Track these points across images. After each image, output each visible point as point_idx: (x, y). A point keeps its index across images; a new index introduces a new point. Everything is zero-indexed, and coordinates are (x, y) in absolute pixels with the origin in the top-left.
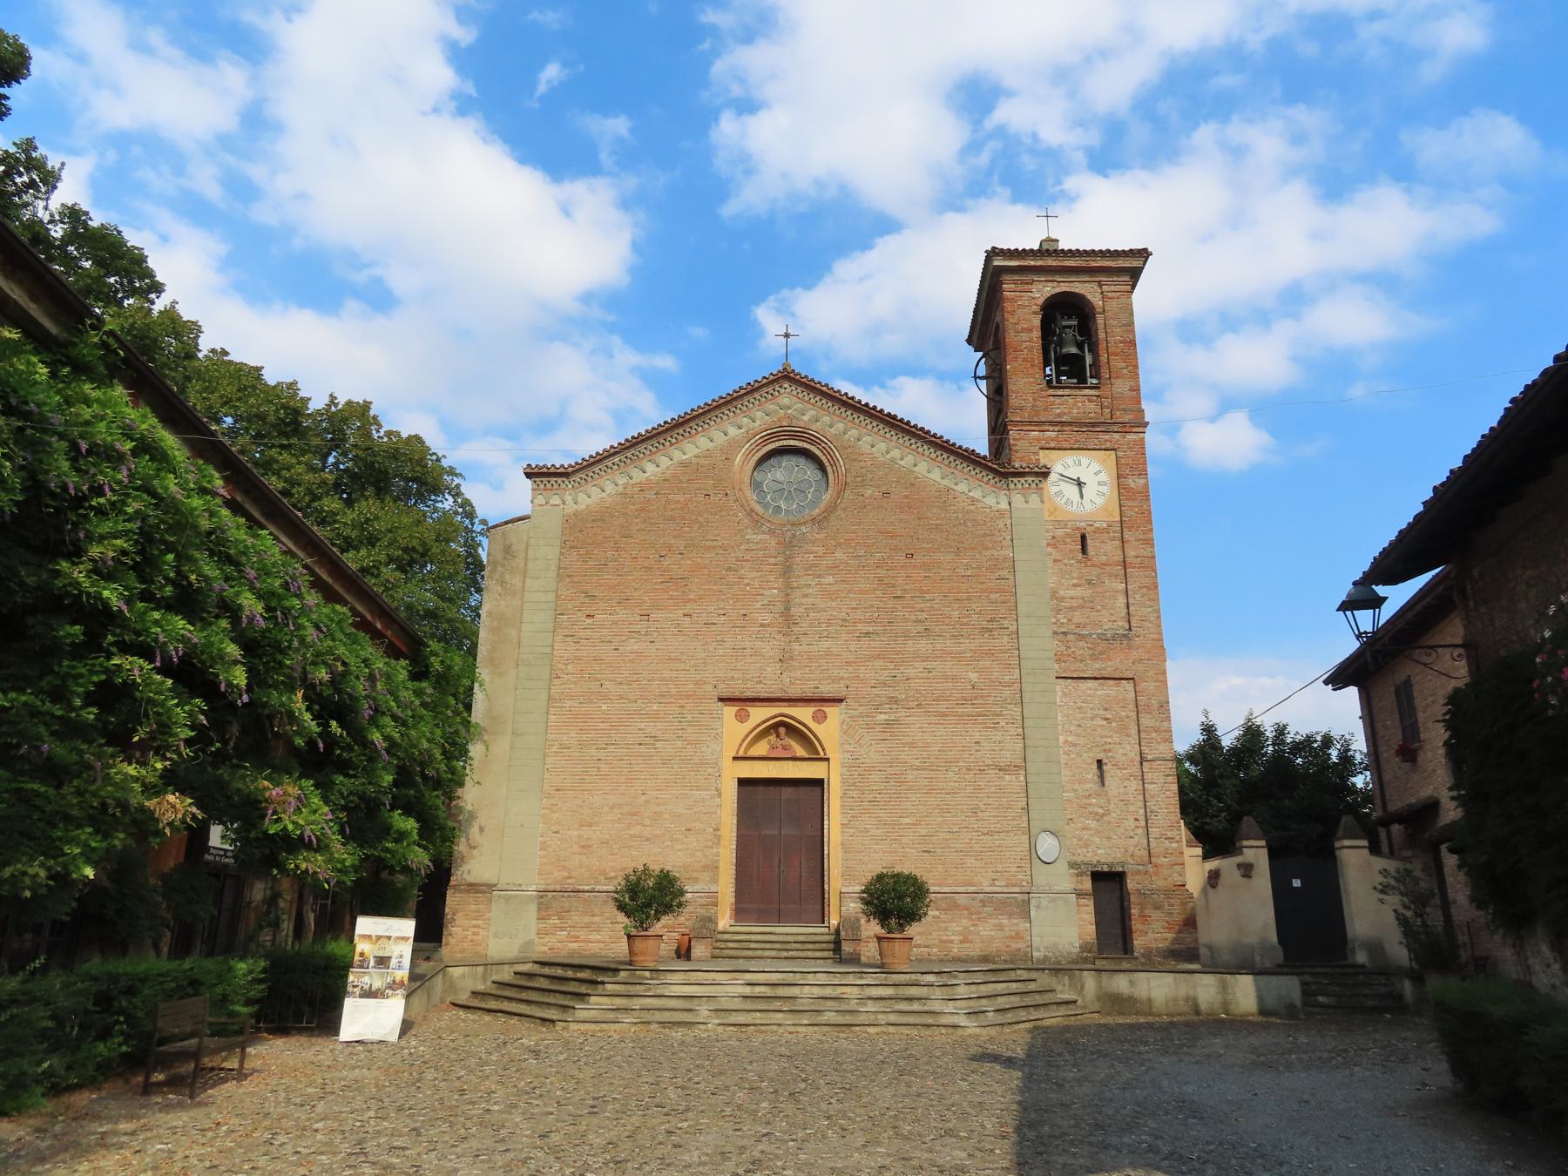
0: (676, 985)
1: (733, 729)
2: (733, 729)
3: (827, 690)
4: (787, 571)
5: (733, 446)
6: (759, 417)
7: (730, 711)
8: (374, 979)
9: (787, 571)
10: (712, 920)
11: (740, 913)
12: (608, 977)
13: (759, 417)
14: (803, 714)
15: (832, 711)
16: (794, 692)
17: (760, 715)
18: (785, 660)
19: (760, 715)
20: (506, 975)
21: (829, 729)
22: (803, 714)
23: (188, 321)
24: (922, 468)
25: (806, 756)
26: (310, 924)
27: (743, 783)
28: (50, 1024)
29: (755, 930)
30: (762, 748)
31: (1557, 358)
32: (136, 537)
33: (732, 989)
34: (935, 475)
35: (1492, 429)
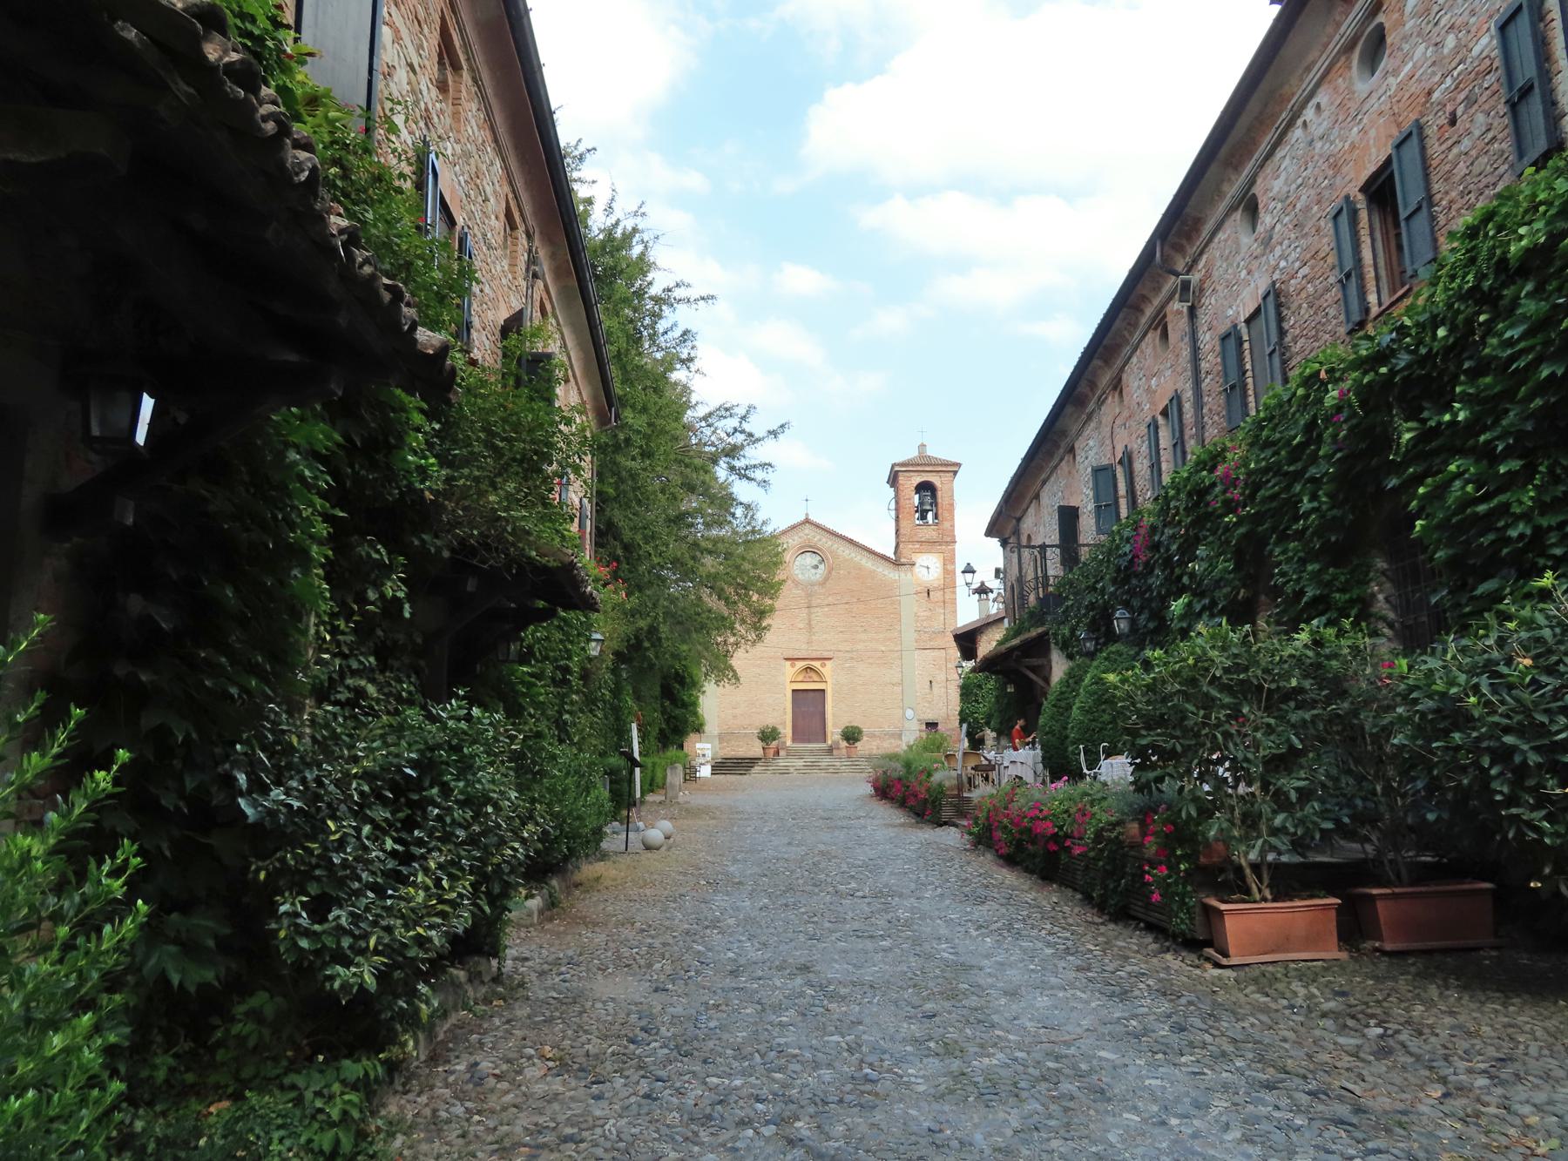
0: (782, 763)
1: (789, 671)
2: (789, 671)
3: (826, 655)
7: (788, 663)
8: (702, 760)
11: (794, 740)
14: (817, 664)
15: (827, 662)
16: (814, 655)
21: (827, 670)
22: (817, 664)
24: (864, 561)
27: (794, 691)
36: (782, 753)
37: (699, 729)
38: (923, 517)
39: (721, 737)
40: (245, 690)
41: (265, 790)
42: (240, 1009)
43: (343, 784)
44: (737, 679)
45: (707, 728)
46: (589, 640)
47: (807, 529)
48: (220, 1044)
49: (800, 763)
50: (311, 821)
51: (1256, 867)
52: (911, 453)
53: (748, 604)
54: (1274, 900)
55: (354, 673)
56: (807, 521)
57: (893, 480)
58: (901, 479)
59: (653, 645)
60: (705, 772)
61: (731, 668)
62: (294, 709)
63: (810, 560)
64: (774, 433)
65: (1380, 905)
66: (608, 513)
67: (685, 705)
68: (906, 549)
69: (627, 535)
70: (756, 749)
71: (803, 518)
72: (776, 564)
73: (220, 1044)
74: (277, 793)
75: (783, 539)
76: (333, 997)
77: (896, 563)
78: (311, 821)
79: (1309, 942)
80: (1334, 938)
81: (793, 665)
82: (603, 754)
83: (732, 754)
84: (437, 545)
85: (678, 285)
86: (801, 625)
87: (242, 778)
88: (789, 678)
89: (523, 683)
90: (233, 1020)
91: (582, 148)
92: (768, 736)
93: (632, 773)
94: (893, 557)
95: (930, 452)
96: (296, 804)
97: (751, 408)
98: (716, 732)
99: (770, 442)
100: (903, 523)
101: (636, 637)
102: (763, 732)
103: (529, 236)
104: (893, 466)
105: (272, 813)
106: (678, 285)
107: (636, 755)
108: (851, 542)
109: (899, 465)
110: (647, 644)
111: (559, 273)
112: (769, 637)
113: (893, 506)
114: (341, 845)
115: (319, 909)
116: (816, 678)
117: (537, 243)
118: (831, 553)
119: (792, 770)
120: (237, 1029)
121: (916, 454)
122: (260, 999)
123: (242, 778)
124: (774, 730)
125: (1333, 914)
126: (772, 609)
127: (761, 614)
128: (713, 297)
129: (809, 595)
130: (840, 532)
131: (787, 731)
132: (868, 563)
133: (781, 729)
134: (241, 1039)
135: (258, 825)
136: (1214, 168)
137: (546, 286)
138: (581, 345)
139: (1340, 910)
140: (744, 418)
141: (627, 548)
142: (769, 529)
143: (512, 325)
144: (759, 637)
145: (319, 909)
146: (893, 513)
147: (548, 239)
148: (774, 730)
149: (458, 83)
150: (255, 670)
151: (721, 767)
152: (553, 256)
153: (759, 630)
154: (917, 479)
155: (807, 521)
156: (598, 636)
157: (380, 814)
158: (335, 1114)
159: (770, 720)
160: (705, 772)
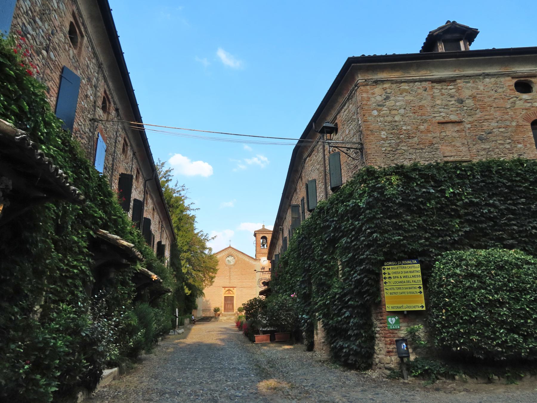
1: (223, 291)
2: (223, 291)
3: (234, 286)
4: (230, 272)
5: (224, 256)
6: (226, 253)
9: (230, 272)
11: (224, 311)
13: (226, 253)
14: (231, 289)
15: (235, 288)
16: (231, 286)
17: (227, 289)
18: (230, 282)
19: (227, 289)
20: (200, 318)
21: (235, 290)
22: (231, 289)
26: (466, 71)
28: (11, 290)
29: (226, 313)
30: (227, 292)
31: (427, 39)
32: (488, 244)
33: (225, 318)
35: (424, 43)
36: (221, 315)
37: (196, 308)
38: (263, 246)
45: (198, 308)
52: (260, 227)
53: (209, 275)
56: (230, 247)
57: (255, 235)
61: (203, 293)
63: (230, 259)
64: (213, 238)
65: (276, 335)
68: (258, 255)
71: (229, 246)
75: (218, 257)
77: (256, 260)
79: (266, 340)
81: (225, 289)
82: (104, 326)
85: (192, 204)
88: (223, 293)
92: (216, 310)
93: (176, 319)
94: (255, 258)
95: (266, 227)
99: (212, 240)
100: (257, 248)
102: (215, 309)
107: (177, 315)
108: (242, 253)
112: (214, 284)
113: (255, 242)
121: (262, 228)
124: (218, 308)
125: (269, 337)
126: (215, 277)
127: (212, 278)
129: (230, 269)
130: (239, 250)
131: (222, 309)
132: (247, 259)
133: (220, 308)
139: (270, 336)
146: (255, 245)
148: (218, 308)
153: (212, 282)
154: (262, 235)
155: (230, 247)
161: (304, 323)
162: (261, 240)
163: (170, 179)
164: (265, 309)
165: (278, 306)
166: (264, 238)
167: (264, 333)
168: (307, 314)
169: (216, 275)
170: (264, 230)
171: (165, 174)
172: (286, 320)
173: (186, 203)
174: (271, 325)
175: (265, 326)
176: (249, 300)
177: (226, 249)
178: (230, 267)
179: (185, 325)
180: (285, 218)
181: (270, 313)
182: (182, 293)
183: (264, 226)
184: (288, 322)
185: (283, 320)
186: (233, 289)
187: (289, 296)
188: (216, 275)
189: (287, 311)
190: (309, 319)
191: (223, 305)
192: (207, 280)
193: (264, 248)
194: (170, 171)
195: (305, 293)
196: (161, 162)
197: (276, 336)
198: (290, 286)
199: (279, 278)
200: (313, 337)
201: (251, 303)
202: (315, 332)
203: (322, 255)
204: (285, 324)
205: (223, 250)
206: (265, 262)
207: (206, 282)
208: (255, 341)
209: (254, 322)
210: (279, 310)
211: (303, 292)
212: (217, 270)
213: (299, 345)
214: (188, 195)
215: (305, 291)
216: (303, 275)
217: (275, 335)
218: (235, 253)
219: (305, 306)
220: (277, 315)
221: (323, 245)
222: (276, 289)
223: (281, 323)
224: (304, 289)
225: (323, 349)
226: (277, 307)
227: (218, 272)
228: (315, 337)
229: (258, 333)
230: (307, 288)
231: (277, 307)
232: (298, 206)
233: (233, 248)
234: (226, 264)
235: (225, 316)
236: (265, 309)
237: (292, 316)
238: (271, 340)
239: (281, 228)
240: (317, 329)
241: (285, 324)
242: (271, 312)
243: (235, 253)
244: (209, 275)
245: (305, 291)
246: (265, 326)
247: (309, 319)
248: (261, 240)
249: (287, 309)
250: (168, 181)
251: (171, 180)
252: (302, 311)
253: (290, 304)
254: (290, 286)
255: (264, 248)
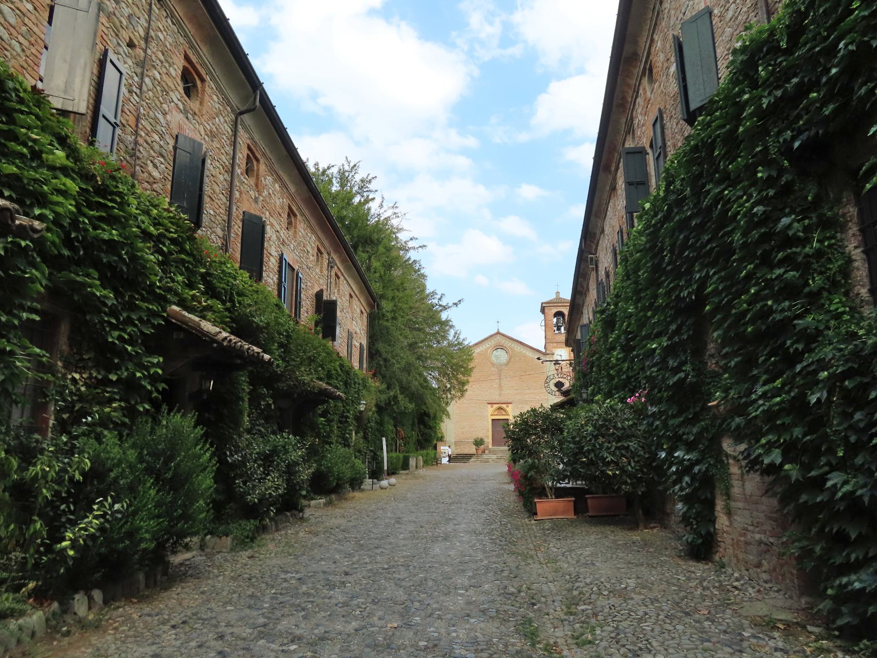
0: (485, 456)
1: (490, 409)
2: (490, 409)
3: (509, 401)
5: (488, 348)
6: (492, 342)
7: (490, 405)
8: (444, 455)
10: (488, 446)
11: (493, 445)
12: (194, 321)
13: (492, 342)
14: (504, 406)
15: (509, 405)
17: (496, 406)
19: (496, 406)
22: (504, 406)
23: (448, 412)
24: (527, 353)
25: (624, 54)
27: (493, 420)
34: (530, 355)
36: (487, 452)
37: (441, 439)
38: (559, 329)
39: (456, 443)
40: (229, 432)
41: (233, 456)
42: (228, 507)
43: (251, 455)
44: (449, 416)
46: (360, 404)
47: (499, 337)
48: (223, 514)
49: (494, 457)
50: (243, 463)
51: (551, 488)
52: (551, 296)
53: (457, 379)
54: (556, 498)
55: (258, 425)
56: (498, 333)
57: (543, 310)
58: (546, 310)
59: (395, 403)
60: (445, 460)
62: (240, 436)
63: (500, 352)
64: (456, 304)
65: (589, 501)
66: (376, 345)
67: (430, 428)
68: (550, 346)
69: (384, 355)
70: (472, 450)
71: (496, 331)
72: (471, 359)
73: (223, 514)
74: (236, 456)
76: (248, 503)
78: (243, 463)
79: (565, 512)
80: (573, 512)
81: (492, 407)
83: (462, 452)
84: (282, 386)
86: (496, 386)
87: (228, 453)
89: (321, 424)
90: (225, 509)
91: (370, 178)
92: (478, 443)
94: (544, 351)
96: (240, 459)
97: (443, 295)
98: (453, 441)
99: (454, 308)
101: (389, 400)
102: (476, 441)
103: (329, 254)
104: (542, 304)
105: (235, 461)
106: (411, 239)
108: (521, 343)
109: (545, 303)
110: (393, 403)
111: (343, 261)
112: (467, 394)
113: (543, 323)
114: (250, 468)
115: (245, 483)
116: (504, 413)
117: (333, 255)
118: (511, 348)
119: (490, 460)
120: (227, 511)
122: (232, 504)
123: (228, 453)
125: (572, 503)
126: (468, 382)
127: (463, 384)
128: (425, 246)
131: (489, 440)
134: (228, 513)
135: (232, 463)
136: (593, 218)
137: (338, 267)
138: (357, 283)
139: (575, 502)
140: (440, 299)
141: (385, 360)
142: (466, 343)
143: (319, 295)
144: (462, 395)
145: (245, 483)
147: (337, 251)
149: (296, 220)
150: (231, 428)
151: (451, 459)
152: (340, 256)
153: (463, 392)
154: (555, 310)
155: (498, 333)
156: (364, 402)
157: (260, 462)
158: (248, 528)
159: (480, 435)
160: (445, 460)
161: (680, 474)
162: (555, 320)
163: (370, 197)
164: (561, 437)
165: (594, 426)
166: (559, 314)
167: (560, 493)
168: (690, 447)
169: (470, 379)
170: (558, 301)
171: (361, 188)
172: (616, 464)
173: (402, 236)
174: (575, 476)
175: (561, 476)
176: (517, 414)
177: (491, 336)
178: (500, 368)
179: (411, 469)
180: (603, 231)
181: (572, 446)
182: (395, 407)
183: (558, 293)
184: (623, 470)
185: (609, 463)
186: (508, 407)
187: (623, 400)
188: (470, 379)
189: (619, 439)
190: (698, 462)
191: (490, 434)
192: (454, 388)
193: (560, 333)
194: (370, 181)
195: (681, 381)
196: (352, 165)
197: (589, 502)
198: (624, 377)
199: (592, 368)
200: (713, 521)
201: (525, 422)
202: (720, 505)
203: (768, 219)
204: (614, 474)
205: (486, 339)
206: (564, 354)
207: (453, 392)
208: (536, 514)
209: (532, 467)
210: (596, 437)
211: (676, 378)
212: (471, 369)
213: (652, 534)
214: (404, 225)
215: (682, 375)
216: (673, 327)
217: (586, 499)
218: (507, 344)
219: (683, 422)
220: (592, 450)
221: (769, 182)
222: (584, 396)
223: (603, 472)
224: (676, 370)
225: (759, 565)
226: (590, 429)
227: (475, 375)
228: (722, 521)
229: (542, 493)
230: (688, 367)
231: (590, 429)
232: (641, 152)
233: (503, 335)
234: (492, 363)
235: (494, 452)
236: (561, 437)
237: (634, 454)
238: (576, 512)
239: (592, 259)
240: (728, 496)
241: (614, 474)
242: (575, 443)
243: (507, 344)
244: (457, 379)
245: (682, 375)
246: (561, 476)
247: (698, 462)
248: (555, 320)
249: (619, 433)
250: (367, 201)
251: (374, 199)
252: (669, 438)
253: (627, 419)
254: (624, 377)
255: (560, 333)
